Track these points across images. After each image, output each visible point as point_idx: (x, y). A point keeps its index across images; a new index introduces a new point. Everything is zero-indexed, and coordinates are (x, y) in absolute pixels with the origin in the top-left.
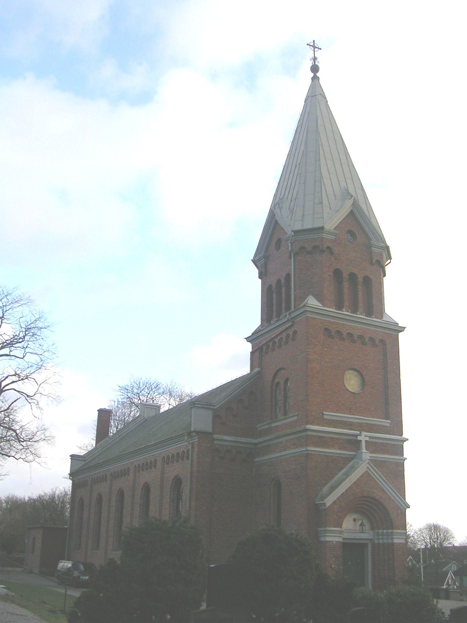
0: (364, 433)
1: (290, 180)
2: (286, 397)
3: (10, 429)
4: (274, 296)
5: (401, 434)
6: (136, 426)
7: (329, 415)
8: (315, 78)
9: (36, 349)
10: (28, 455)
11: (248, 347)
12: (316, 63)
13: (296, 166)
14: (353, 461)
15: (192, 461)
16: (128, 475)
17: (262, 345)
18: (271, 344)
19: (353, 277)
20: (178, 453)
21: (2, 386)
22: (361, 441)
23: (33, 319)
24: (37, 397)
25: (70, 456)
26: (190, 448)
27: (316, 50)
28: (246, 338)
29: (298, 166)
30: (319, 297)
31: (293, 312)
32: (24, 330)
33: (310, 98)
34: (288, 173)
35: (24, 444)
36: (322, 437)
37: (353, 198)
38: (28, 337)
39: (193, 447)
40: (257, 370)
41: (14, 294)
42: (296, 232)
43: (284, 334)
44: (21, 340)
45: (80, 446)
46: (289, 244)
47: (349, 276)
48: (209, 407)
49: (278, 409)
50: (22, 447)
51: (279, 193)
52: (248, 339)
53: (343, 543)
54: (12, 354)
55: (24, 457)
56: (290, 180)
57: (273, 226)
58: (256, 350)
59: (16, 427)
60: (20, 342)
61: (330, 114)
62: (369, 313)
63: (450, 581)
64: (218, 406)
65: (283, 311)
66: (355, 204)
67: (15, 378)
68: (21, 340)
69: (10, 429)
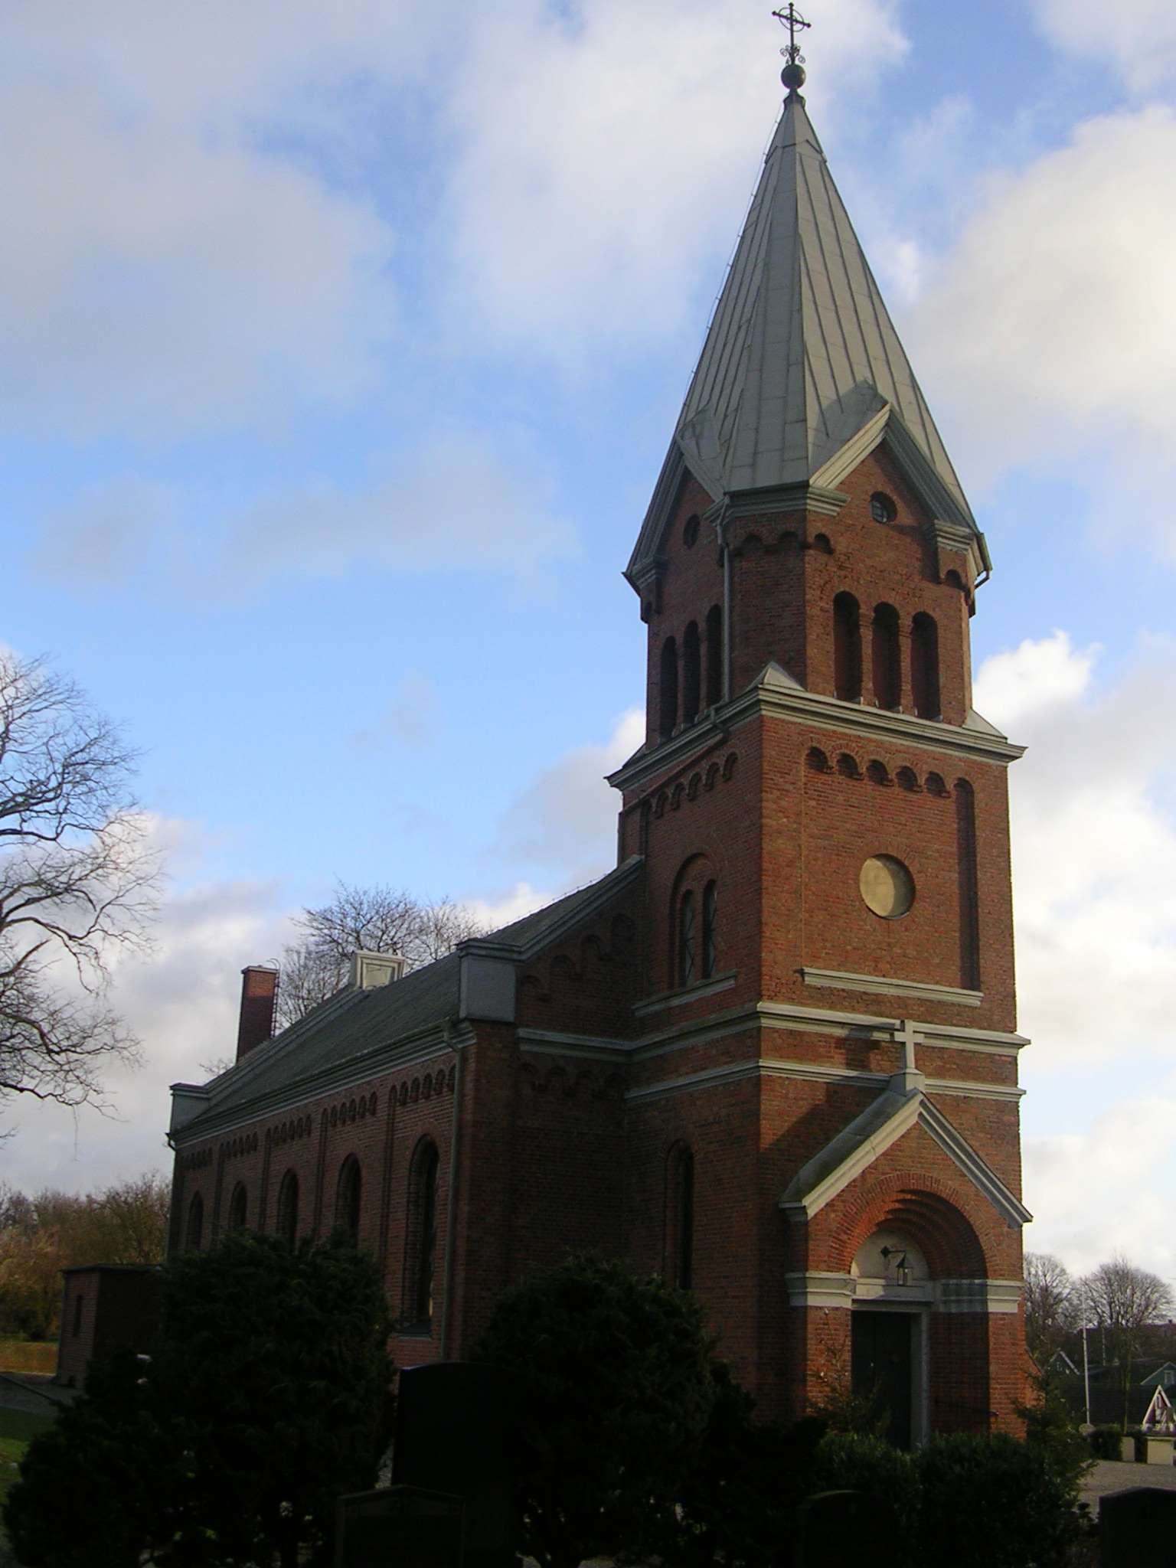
0: (911, 1025)
1: (724, 362)
2: (707, 931)
3: (18, 1018)
4: (681, 663)
5: (1013, 1029)
6: (341, 1011)
7: (817, 976)
8: (793, 101)
9: (91, 814)
10: (68, 1086)
11: (615, 800)
12: (797, 62)
13: (740, 327)
14: (880, 1099)
15: (462, 1095)
16: (309, 1134)
17: (649, 794)
18: (670, 791)
19: (886, 615)
20: (429, 1075)
21: (5, 911)
22: (903, 1044)
23: (84, 741)
24: (95, 939)
25: (172, 1088)
26: (457, 1061)
27: (797, 27)
28: (608, 778)
29: (744, 327)
30: (797, 669)
31: (726, 706)
32: (59, 768)
33: (779, 151)
34: (720, 346)
35: (61, 1058)
36: (800, 1034)
37: (887, 408)
38: (70, 786)
39: (464, 1060)
40: (634, 859)
41: (33, 675)
42: (735, 496)
43: (705, 765)
44: (51, 795)
45: (207, 1064)
46: (719, 529)
47: (876, 610)
48: (507, 955)
49: (688, 962)
50: (57, 1068)
51: (695, 400)
52: (613, 780)
53: (853, 1312)
54: (26, 827)
55: (58, 1091)
56: (724, 362)
57: (678, 482)
58: (637, 806)
59: (36, 1015)
60: (50, 800)
61: (831, 193)
62: (929, 708)
63: (1158, 1412)
64: (529, 954)
65: (703, 704)
66: (894, 425)
67: (34, 892)
68: (51, 795)
69: (18, 1018)
